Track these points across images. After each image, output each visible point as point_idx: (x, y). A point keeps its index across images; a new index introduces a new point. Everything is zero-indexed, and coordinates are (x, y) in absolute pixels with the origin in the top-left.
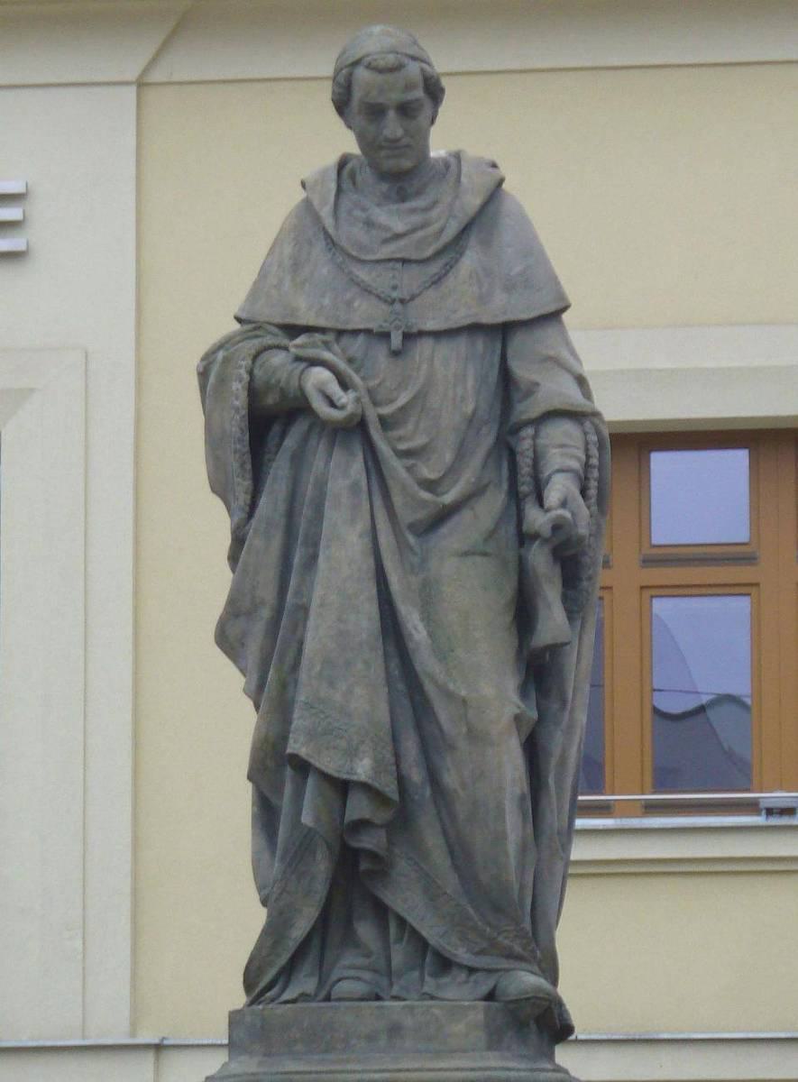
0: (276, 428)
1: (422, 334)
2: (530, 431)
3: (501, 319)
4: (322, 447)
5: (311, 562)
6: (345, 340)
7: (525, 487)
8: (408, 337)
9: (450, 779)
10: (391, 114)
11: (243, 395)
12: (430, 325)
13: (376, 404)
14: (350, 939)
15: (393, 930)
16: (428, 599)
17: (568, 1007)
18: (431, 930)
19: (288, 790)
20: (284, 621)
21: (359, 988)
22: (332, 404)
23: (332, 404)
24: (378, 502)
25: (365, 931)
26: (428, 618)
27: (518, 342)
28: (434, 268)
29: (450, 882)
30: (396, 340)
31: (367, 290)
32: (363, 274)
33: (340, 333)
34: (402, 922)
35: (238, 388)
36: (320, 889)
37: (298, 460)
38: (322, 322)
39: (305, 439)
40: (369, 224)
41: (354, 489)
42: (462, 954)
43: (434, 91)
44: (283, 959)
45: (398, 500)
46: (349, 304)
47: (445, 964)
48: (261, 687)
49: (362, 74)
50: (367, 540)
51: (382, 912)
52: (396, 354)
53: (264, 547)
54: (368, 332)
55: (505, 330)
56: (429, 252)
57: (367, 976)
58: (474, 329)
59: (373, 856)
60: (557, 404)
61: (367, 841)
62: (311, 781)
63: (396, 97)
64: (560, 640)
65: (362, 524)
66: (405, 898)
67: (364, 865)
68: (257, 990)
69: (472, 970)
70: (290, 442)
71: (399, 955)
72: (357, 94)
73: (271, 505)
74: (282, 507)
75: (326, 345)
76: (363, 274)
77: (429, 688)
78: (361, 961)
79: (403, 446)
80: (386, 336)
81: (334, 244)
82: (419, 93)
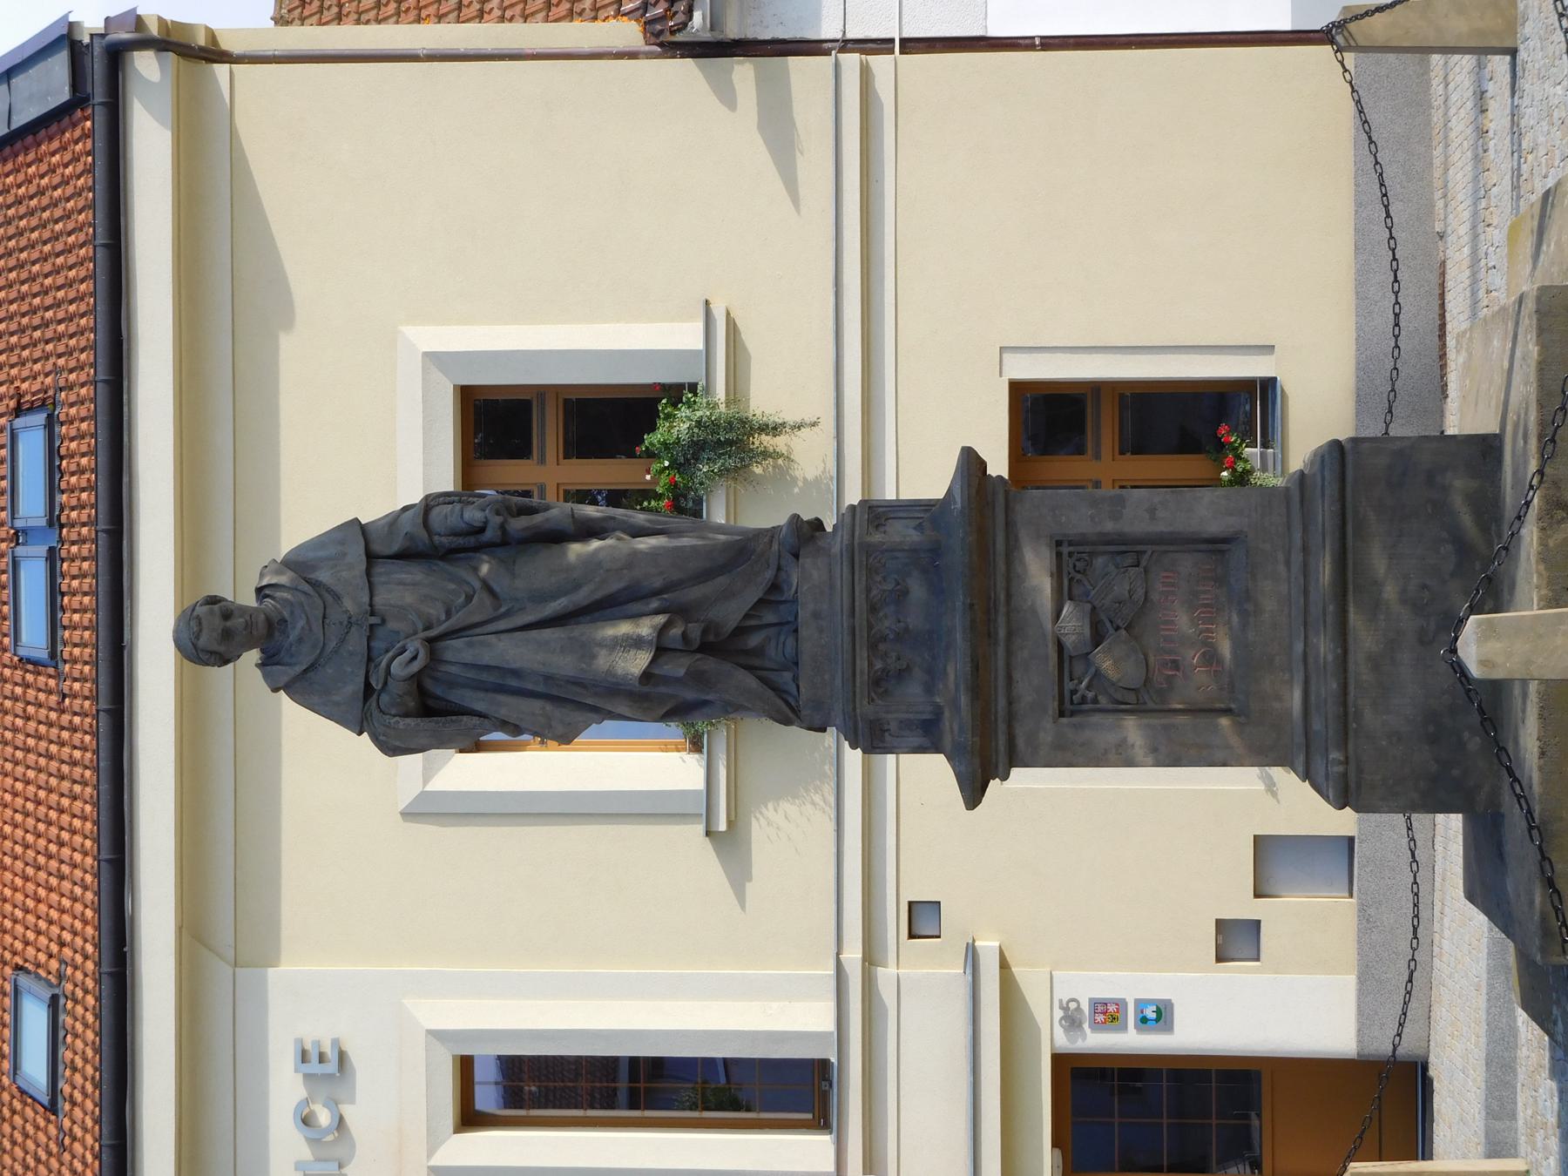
0: (430, 702)
1: (371, 605)
2: (436, 538)
3: (364, 558)
4: (444, 668)
5: (516, 673)
6: (375, 653)
7: (472, 541)
8: (372, 614)
9: (658, 583)
10: (229, 624)
11: (408, 720)
12: (366, 599)
13: (415, 633)
14: (759, 652)
15: (753, 622)
16: (541, 597)
17: (743, 337)
18: (753, 594)
19: (663, 689)
20: (554, 692)
21: (790, 642)
22: (415, 658)
23: (415, 658)
24: (478, 630)
25: (754, 641)
26: (554, 596)
27: (377, 548)
28: (326, 595)
29: (722, 581)
30: (373, 620)
31: (342, 641)
32: (332, 645)
33: (370, 659)
34: (747, 616)
35: (404, 723)
36: (727, 667)
37: (453, 684)
38: (363, 672)
39: (435, 679)
40: (300, 640)
41: (470, 645)
42: (769, 574)
43: (213, 600)
44: (770, 693)
45: (476, 619)
46: (351, 654)
47: (775, 587)
48: (595, 709)
49: (202, 642)
50: (503, 636)
51: (741, 631)
52: (384, 621)
53: (509, 706)
54: (369, 639)
55: (371, 557)
56: (319, 602)
57: (782, 638)
58: (368, 573)
59: (705, 632)
60: (420, 520)
61: (695, 630)
62: (656, 671)
63: (218, 622)
64: (750, 888)
65: (492, 638)
66: (731, 613)
67: (711, 638)
68: (791, 715)
69: (779, 568)
70: (438, 691)
71: (770, 617)
72: (216, 647)
73: (479, 702)
74: (481, 695)
75: (377, 666)
76: (332, 645)
77: (598, 595)
78: (773, 644)
79: (443, 617)
80: (371, 626)
81: (312, 665)
82: (216, 607)
